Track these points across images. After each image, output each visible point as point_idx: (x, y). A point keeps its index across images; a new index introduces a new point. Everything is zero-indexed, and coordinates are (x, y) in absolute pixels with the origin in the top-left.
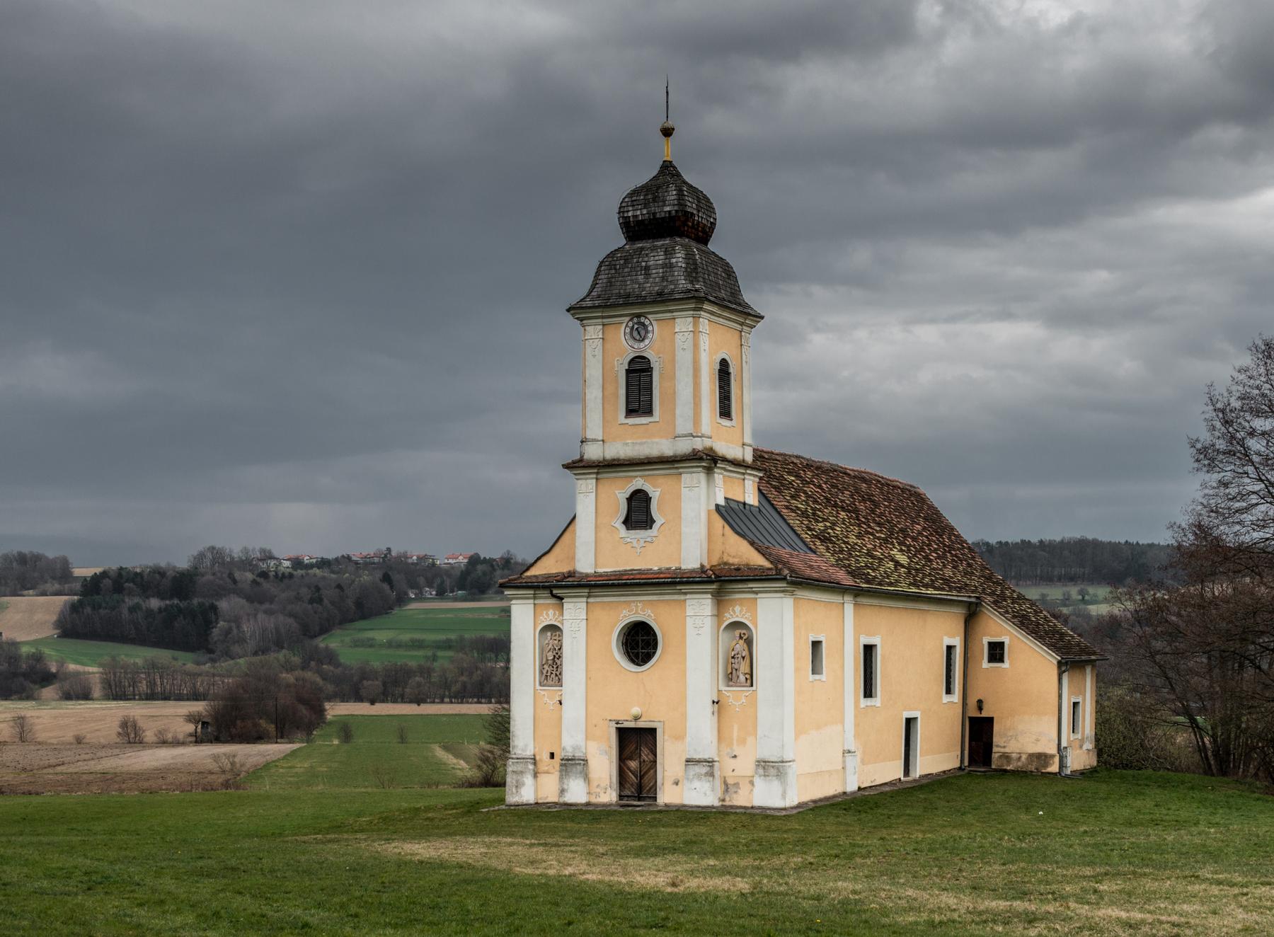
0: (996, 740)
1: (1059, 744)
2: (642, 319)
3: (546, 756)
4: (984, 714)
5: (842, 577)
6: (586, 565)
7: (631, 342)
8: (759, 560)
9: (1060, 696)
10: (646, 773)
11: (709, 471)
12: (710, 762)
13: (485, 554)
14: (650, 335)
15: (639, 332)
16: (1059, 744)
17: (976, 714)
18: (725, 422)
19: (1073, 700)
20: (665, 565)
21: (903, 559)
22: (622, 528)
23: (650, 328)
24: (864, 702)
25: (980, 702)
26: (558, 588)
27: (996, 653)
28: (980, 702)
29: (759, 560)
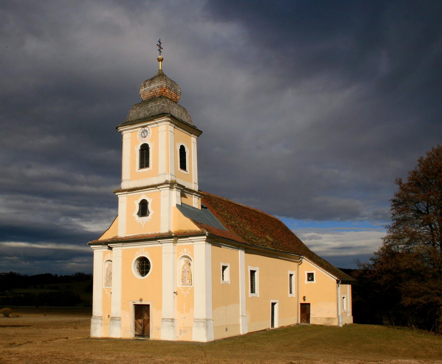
0: (132, 338)
1: (338, 314)
2: (146, 128)
3: (107, 317)
4: (306, 302)
5: (234, 236)
6: (122, 234)
7: (141, 138)
8: (198, 229)
9: (337, 294)
10: (146, 325)
11: (171, 188)
12: (173, 320)
13: (347, 323)
14: (149, 134)
15: (144, 134)
16: (338, 314)
17: (303, 302)
18: (183, 171)
19: (343, 296)
20: (153, 233)
21: (271, 239)
22: (137, 216)
23: (149, 132)
24: (250, 295)
25: (304, 297)
26: (109, 244)
27: (311, 277)
28: (304, 297)
29: (198, 229)
